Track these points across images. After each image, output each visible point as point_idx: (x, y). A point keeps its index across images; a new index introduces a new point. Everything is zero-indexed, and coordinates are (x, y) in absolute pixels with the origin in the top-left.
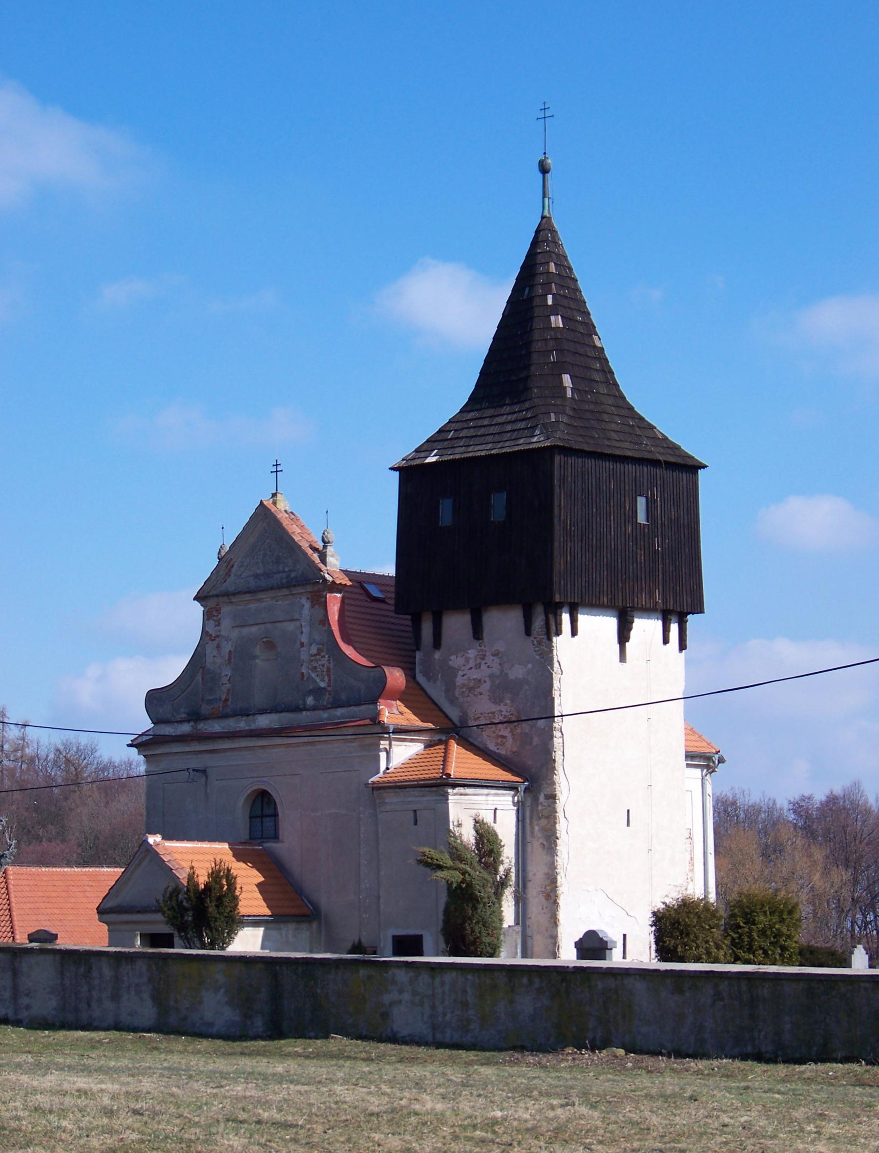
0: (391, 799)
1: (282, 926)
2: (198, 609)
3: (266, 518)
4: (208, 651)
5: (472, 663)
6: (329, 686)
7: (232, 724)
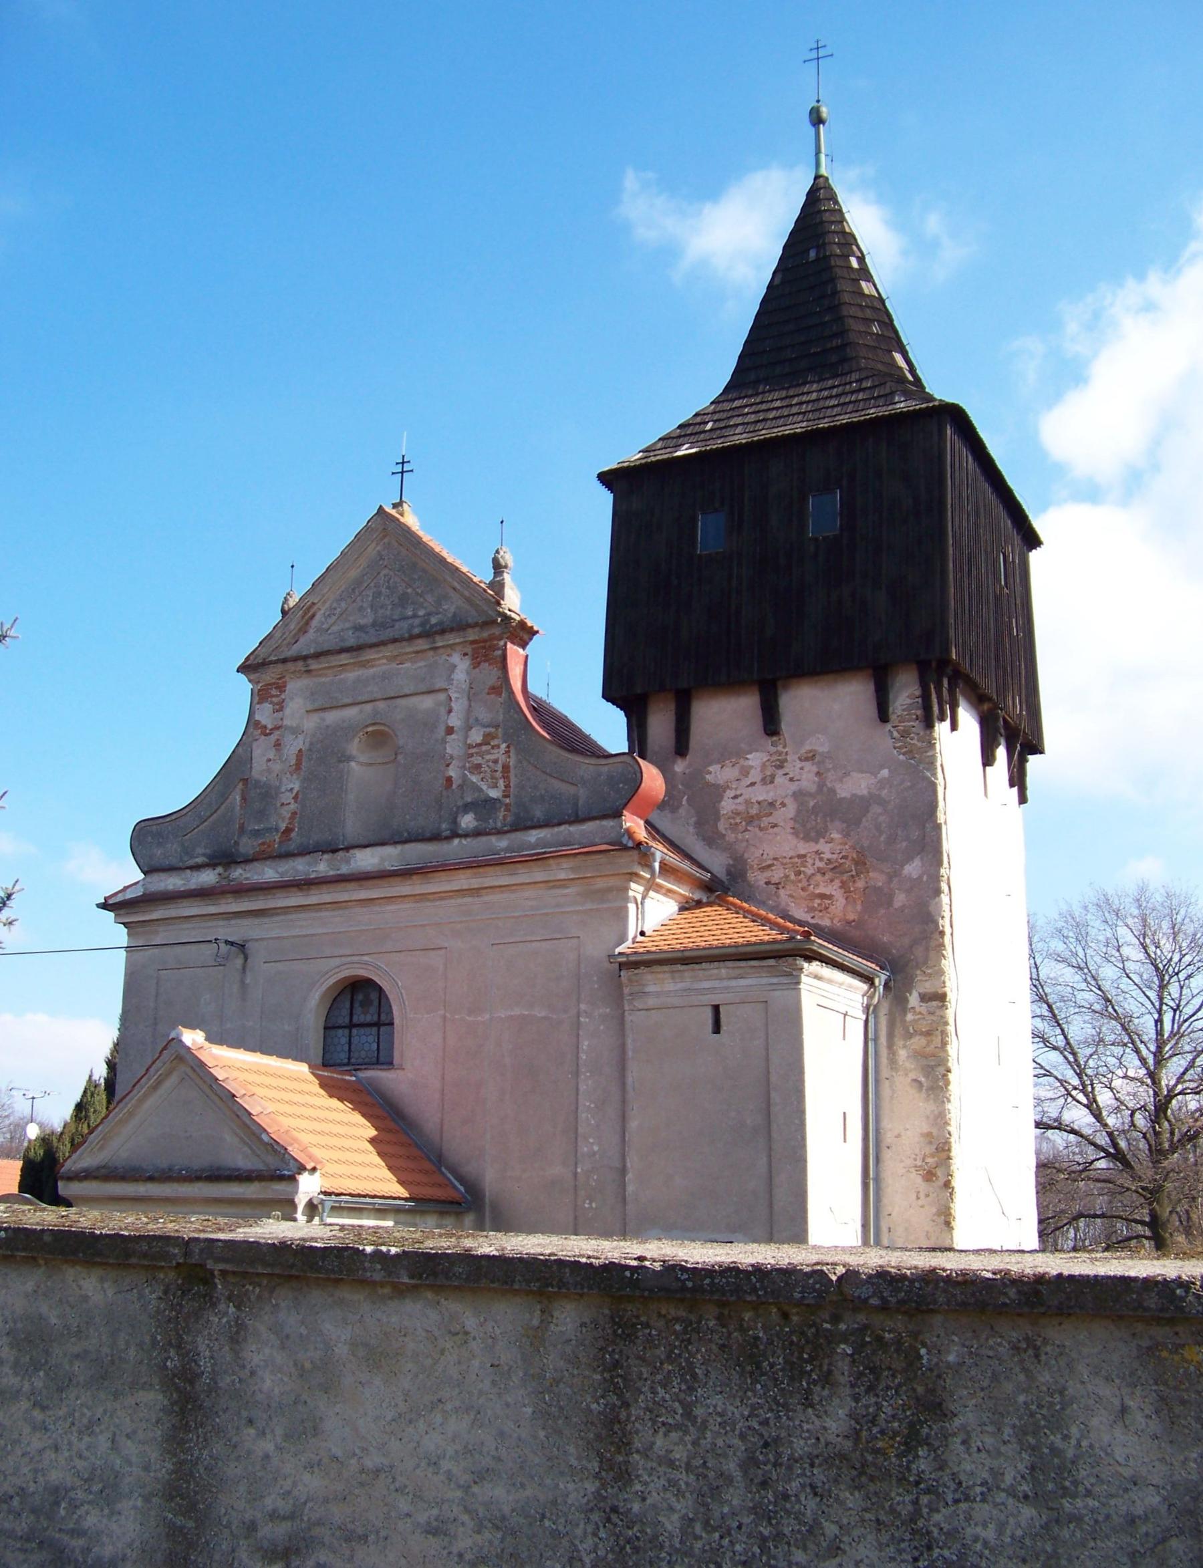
0: (660, 984)
2: (243, 687)
3: (385, 536)
4: (257, 753)
5: (755, 775)
6: (506, 796)
7: (300, 868)
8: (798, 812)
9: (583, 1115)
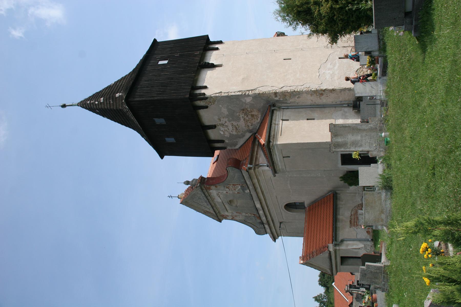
1: (338, 207)
2: (224, 221)
5: (226, 129)
6: (240, 185)
8: (233, 121)
9: (312, 176)
